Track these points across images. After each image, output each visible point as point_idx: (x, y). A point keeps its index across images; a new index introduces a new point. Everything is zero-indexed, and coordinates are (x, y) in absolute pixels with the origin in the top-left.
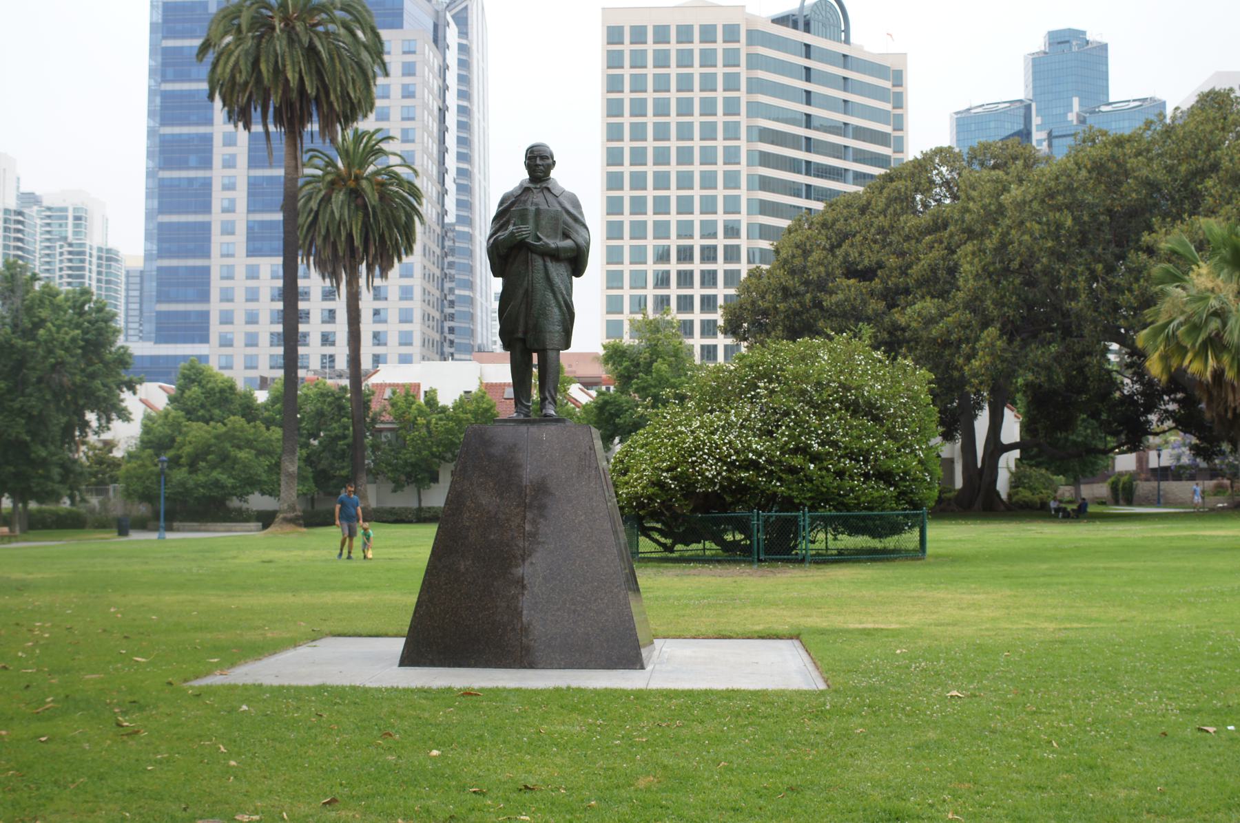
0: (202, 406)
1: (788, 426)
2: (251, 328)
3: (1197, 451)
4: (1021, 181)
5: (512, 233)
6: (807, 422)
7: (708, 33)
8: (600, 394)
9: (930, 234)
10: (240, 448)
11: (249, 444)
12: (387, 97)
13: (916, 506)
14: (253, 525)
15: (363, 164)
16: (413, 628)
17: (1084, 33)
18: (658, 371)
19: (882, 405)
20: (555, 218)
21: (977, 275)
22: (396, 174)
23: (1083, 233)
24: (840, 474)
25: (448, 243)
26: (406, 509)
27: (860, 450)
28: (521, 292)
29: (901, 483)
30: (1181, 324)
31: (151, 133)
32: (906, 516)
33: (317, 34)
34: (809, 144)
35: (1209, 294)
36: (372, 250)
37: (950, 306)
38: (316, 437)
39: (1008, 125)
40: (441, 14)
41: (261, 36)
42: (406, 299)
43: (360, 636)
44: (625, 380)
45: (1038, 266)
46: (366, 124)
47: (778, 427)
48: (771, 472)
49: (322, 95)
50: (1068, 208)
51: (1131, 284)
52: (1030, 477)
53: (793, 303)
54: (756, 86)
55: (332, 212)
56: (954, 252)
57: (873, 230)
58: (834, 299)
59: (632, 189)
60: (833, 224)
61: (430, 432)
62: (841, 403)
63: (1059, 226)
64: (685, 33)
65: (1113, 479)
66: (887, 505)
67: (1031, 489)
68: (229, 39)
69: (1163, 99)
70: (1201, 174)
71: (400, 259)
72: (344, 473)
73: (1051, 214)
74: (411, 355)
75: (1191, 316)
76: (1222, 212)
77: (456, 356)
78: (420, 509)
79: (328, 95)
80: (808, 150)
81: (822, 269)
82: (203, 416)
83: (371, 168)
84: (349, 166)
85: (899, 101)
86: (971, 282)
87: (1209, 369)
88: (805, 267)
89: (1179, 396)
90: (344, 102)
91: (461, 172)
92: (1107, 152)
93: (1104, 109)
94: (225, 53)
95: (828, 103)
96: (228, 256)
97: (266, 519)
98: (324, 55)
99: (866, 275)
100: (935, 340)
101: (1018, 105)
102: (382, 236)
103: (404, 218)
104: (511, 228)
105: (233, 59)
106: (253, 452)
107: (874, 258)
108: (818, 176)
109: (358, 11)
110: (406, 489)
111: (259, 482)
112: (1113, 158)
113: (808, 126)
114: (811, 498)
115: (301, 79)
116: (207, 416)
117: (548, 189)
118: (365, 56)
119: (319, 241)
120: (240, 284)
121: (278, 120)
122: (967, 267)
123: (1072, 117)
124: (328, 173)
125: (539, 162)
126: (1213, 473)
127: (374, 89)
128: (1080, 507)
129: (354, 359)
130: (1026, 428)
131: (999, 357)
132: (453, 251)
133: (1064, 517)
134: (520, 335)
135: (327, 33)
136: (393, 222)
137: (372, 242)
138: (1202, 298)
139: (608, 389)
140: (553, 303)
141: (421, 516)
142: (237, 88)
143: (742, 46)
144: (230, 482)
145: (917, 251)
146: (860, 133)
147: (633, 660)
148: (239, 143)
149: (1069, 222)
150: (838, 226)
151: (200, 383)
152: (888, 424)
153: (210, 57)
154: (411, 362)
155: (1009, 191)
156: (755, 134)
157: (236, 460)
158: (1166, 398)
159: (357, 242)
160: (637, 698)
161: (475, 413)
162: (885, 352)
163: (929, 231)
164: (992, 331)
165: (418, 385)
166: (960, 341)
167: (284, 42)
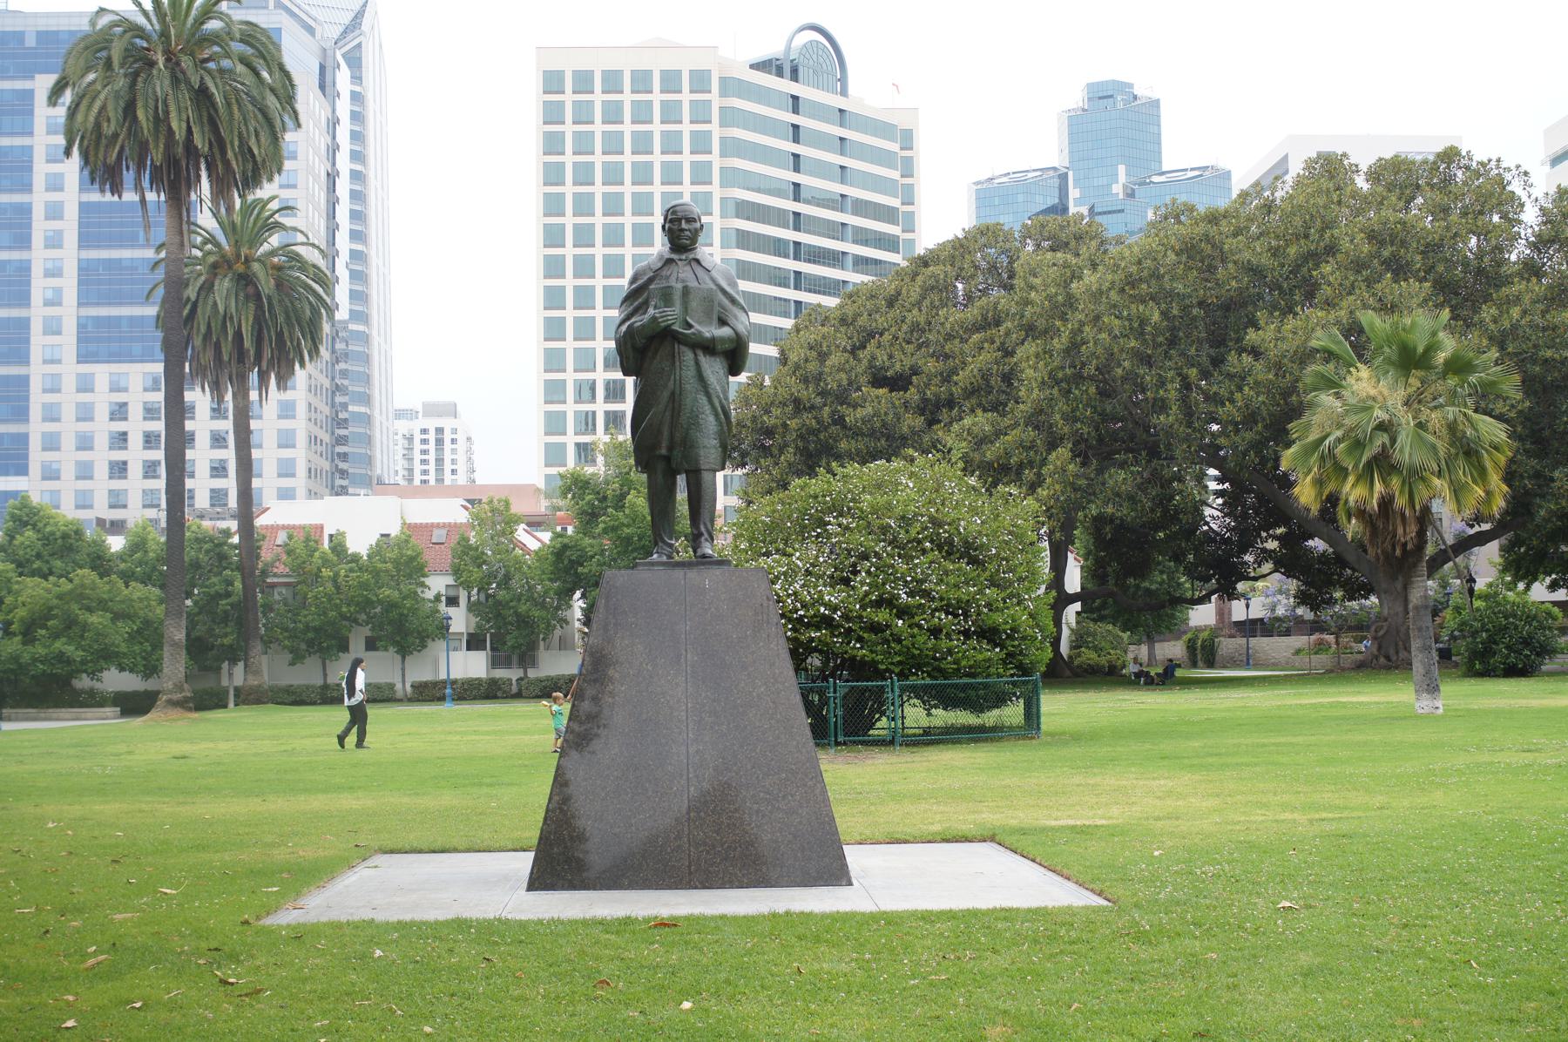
0: (39, 556)
1: (868, 572)
2: (84, 456)
3: (1302, 598)
4: (1094, 266)
5: (654, 319)
6: (892, 566)
7: (671, 81)
8: (557, 536)
9: (978, 330)
10: (90, 610)
11: (103, 605)
12: (295, 158)
13: (1025, 670)
14: (109, 711)
15: (256, 240)
16: (543, 839)
17: (1131, 86)
18: (633, 505)
19: (982, 545)
20: (709, 300)
21: (1043, 383)
22: (298, 255)
23: (1173, 329)
24: (935, 632)
25: (339, 346)
26: (308, 687)
27: (959, 601)
28: (666, 394)
29: (1008, 642)
30: (1339, 440)
32: (1014, 684)
33: (209, 71)
34: (798, 221)
35: (1370, 403)
36: (267, 353)
37: (1007, 421)
38: (189, 595)
39: (1039, 199)
40: (329, 53)
41: (136, 74)
42: (287, 417)
43: (421, 852)
44: (589, 517)
45: (1119, 371)
46: (265, 191)
47: (855, 573)
48: (849, 630)
49: (216, 150)
50: (1152, 299)
51: (1232, 393)
52: (1094, 635)
53: (808, 419)
54: (731, 148)
55: (215, 304)
56: (1011, 354)
57: (905, 327)
58: (860, 413)
59: (575, 276)
60: (854, 320)
61: (338, 587)
62: (932, 542)
63: (1143, 322)
64: (642, 81)
65: (1189, 635)
66: (993, 670)
67: (1096, 649)
68: (91, 77)
69: (1228, 168)
70: (1315, 258)
71: (302, 365)
72: (226, 641)
73: (1133, 306)
74: (294, 489)
75: (1352, 430)
76: (1344, 304)
77: (351, 490)
78: (326, 687)
79: (223, 152)
80: (797, 228)
81: (844, 376)
82: (39, 569)
83: (265, 247)
84: (237, 245)
85: (908, 169)
86: (1036, 391)
87: (1376, 496)
88: (821, 374)
89: (1280, 531)
90: (245, 160)
91: (356, 256)
92: (1201, 229)
93: (1156, 179)
95: (821, 169)
96: (52, 362)
97: (134, 705)
98: (218, 99)
99: (898, 383)
100: (990, 464)
101: (1051, 173)
102: (280, 335)
103: (308, 312)
104: (651, 311)
106: (108, 615)
107: (908, 362)
108: (809, 261)
109: (263, 44)
110: (308, 661)
111: (117, 654)
112: (1207, 238)
113: (797, 198)
114: (900, 663)
115: (189, 131)
116: (45, 569)
117: (698, 261)
119: (198, 341)
120: (69, 399)
121: (156, 181)
122: (1030, 372)
123: (1117, 189)
124: (209, 253)
125: (684, 225)
126: (1316, 627)
127: (283, 145)
128: (1166, 670)
129: (246, 494)
130: (1091, 574)
131: (1072, 484)
132: (346, 356)
133: (1146, 683)
134: (664, 451)
135: (221, 71)
136: (293, 316)
137: (266, 342)
138: (1365, 408)
139: (565, 529)
140: (707, 409)
141: (546, 690)
142: (104, 141)
143: (714, 98)
144: (78, 655)
145: (962, 353)
146: (861, 208)
147: (837, 874)
148: (67, 215)
149: (1156, 317)
150: (861, 321)
151: (34, 526)
152: (992, 567)
153: (68, 97)
154: (293, 497)
155: (1080, 278)
156: (731, 208)
157: (85, 627)
158: (1264, 534)
159: (248, 343)
160: (888, 923)
161: (396, 563)
162: (980, 477)
163: (977, 328)
164: (1063, 453)
165: (322, 527)
166: (1021, 466)
167: (167, 82)
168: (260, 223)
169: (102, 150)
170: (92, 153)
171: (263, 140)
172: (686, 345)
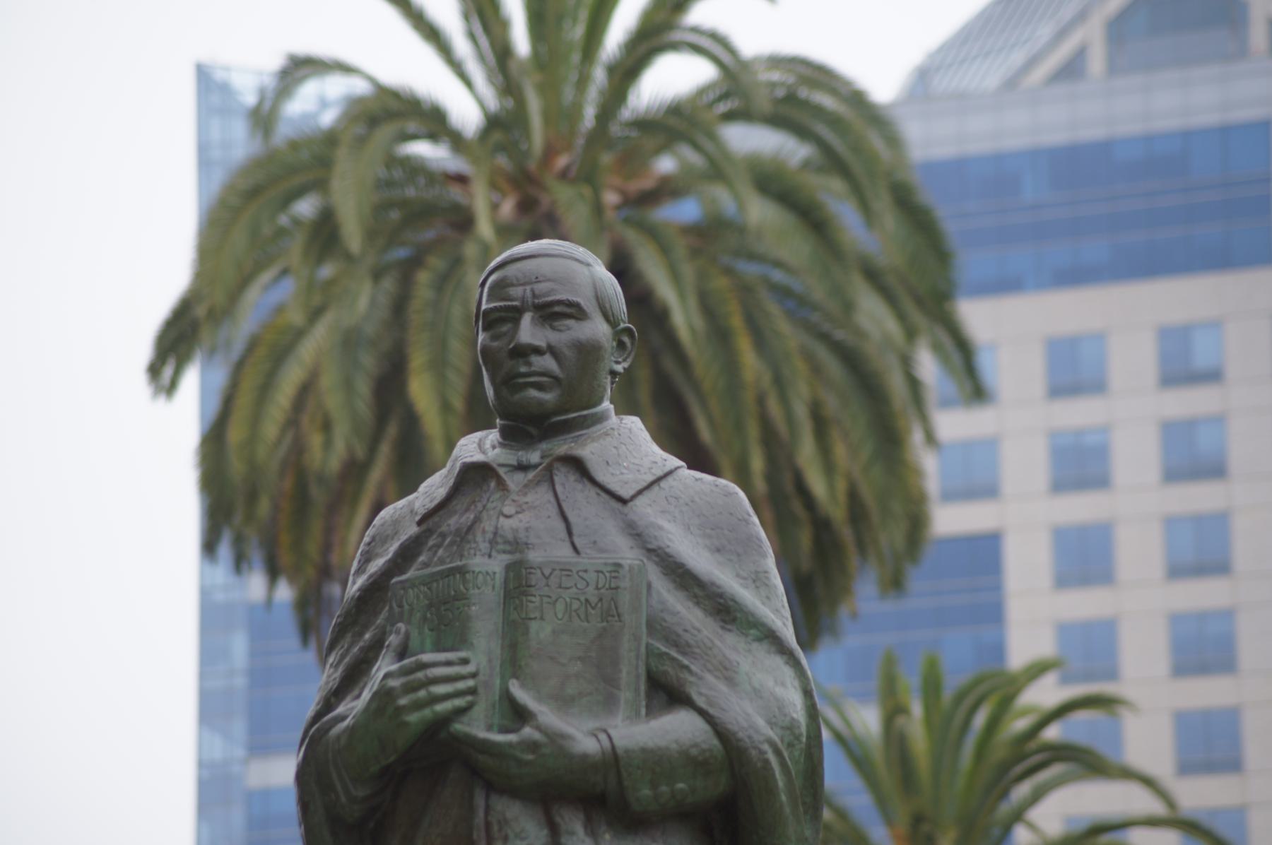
12: (987, 490)
20: (606, 606)
33: (653, 233)
94: (275, 347)
105: (291, 378)
117: (578, 466)
118: (874, 316)
125: (528, 331)
168: (999, 752)
169: (316, 527)
170: (285, 539)
171: (840, 451)
172: (514, 792)
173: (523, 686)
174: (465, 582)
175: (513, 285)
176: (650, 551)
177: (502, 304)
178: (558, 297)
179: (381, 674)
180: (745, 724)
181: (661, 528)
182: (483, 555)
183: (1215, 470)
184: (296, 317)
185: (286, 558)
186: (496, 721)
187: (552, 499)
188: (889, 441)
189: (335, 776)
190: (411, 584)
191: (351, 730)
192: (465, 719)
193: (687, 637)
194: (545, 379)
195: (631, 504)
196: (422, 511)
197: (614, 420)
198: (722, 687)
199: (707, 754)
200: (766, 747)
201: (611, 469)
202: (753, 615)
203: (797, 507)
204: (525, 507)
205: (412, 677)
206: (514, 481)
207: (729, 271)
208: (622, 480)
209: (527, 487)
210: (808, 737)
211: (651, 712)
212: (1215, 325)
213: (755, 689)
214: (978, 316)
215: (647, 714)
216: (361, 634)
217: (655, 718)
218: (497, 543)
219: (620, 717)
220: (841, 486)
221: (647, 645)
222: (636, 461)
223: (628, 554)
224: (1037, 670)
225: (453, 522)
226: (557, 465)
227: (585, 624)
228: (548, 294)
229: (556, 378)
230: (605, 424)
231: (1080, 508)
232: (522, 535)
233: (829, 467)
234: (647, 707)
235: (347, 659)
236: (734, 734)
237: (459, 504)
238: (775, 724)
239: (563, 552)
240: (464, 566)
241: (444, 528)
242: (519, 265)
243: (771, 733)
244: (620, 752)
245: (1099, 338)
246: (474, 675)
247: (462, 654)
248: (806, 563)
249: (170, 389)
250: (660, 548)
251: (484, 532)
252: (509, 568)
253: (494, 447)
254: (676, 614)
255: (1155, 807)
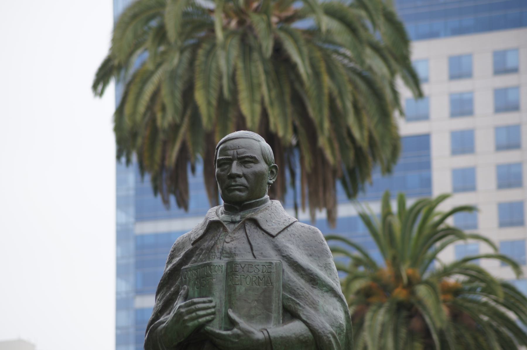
20: (267, 279)
31: (122, 234)
33: (291, 34)
84: (395, 262)
90: (343, 148)
94: (143, 77)
105: (149, 89)
117: (255, 222)
118: (377, 65)
125: (235, 168)
142: (161, 136)
167: (235, 52)
168: (427, 231)
171: (366, 120)
173: (234, 311)
174: (211, 269)
175: (229, 150)
176: (283, 256)
177: (225, 157)
178: (247, 155)
179: (178, 306)
180: (321, 326)
181: (288, 247)
182: (218, 258)
183: (515, 107)
184: (150, 66)
185: (146, 163)
186: (223, 326)
187: (245, 236)
188: (385, 116)
189: (160, 346)
190: (189, 269)
191: (166, 328)
192: (211, 324)
193: (298, 291)
194: (242, 187)
195: (276, 237)
196: (194, 239)
197: (270, 202)
198: (312, 311)
199: (307, 339)
200: (330, 335)
201: (268, 223)
202: (324, 282)
203: (348, 142)
204: (234, 239)
205: (190, 308)
206: (230, 228)
207: (321, 49)
208: (272, 228)
209: (235, 230)
210: (347, 330)
211: (284, 322)
212: (516, 50)
213: (325, 312)
214: (420, 52)
215: (283, 323)
216: (170, 288)
217: (286, 324)
218: (223, 253)
219: (272, 324)
220: (366, 134)
221: (283, 294)
222: (278, 220)
223: (275, 258)
224: (443, 198)
225: (206, 244)
226: (247, 222)
227: (258, 287)
228: (243, 153)
229: (246, 187)
230: (266, 204)
231: (461, 124)
232: (233, 250)
233: (361, 127)
234: (283, 320)
235: (164, 298)
236: (317, 330)
237: (209, 237)
238: (334, 326)
239: (249, 257)
240: (211, 263)
241: (202, 247)
242: (231, 142)
243: (332, 330)
244: (272, 338)
245: (470, 56)
246: (214, 307)
247: (210, 299)
248: (351, 165)
249: (101, 94)
250: (288, 255)
251: (218, 249)
252: (228, 264)
253: (222, 214)
254: (294, 282)
255: (489, 250)
